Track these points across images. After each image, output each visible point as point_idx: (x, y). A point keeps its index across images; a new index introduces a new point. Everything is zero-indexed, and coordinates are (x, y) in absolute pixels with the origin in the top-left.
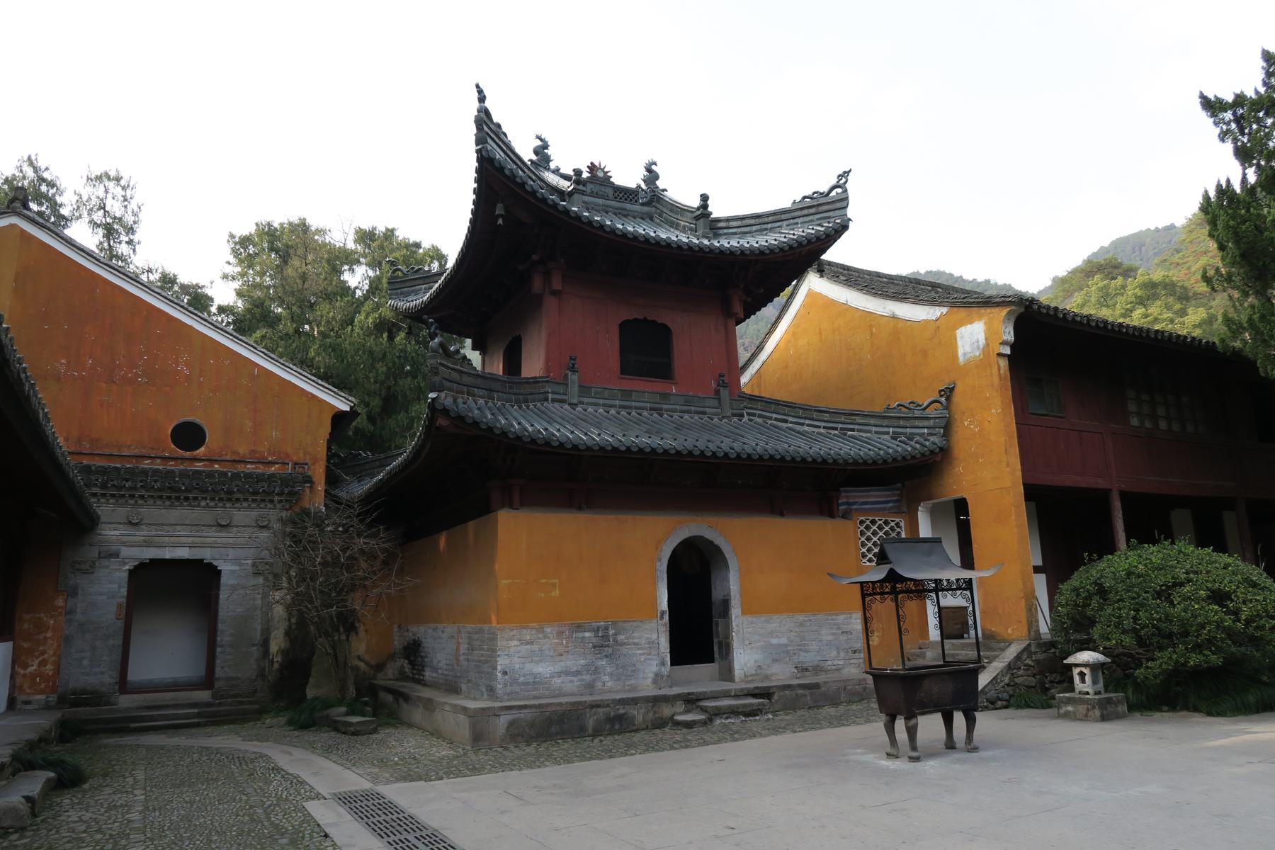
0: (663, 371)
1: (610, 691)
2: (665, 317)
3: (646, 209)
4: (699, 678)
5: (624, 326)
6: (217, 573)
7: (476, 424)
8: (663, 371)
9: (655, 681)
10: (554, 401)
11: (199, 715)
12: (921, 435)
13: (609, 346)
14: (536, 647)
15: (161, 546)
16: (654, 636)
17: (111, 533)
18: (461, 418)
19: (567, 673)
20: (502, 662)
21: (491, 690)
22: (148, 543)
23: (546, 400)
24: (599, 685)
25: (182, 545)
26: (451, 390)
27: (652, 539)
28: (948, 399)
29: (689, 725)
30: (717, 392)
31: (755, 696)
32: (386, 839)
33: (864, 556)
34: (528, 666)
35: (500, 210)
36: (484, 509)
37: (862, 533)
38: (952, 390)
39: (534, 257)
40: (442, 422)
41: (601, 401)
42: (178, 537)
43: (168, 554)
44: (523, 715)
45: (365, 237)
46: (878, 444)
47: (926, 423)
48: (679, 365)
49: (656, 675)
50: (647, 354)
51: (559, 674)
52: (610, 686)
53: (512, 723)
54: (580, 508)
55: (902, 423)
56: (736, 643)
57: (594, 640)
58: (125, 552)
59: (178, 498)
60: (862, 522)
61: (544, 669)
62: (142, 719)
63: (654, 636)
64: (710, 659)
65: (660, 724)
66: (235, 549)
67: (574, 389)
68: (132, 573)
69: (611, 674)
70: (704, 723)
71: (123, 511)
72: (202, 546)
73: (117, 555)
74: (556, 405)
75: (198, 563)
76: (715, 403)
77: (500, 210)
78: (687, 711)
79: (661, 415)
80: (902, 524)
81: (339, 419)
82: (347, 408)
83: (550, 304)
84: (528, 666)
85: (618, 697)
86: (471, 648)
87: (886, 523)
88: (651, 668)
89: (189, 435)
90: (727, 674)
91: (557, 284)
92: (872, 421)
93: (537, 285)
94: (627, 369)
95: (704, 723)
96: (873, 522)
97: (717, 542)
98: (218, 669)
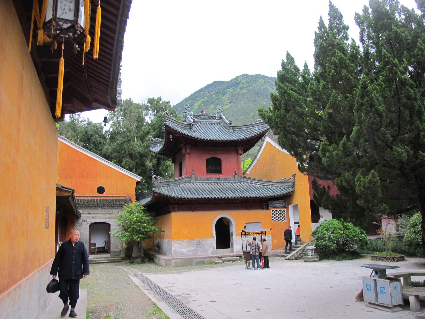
0: (219, 171)
1: (200, 255)
2: (219, 156)
3: (218, 121)
4: (224, 252)
5: (208, 160)
6: (109, 225)
7: (163, 195)
8: (219, 171)
9: (212, 253)
10: (188, 182)
11: (108, 260)
12: (287, 187)
13: (203, 166)
14: (181, 245)
15: (96, 219)
16: (212, 242)
17: (83, 216)
18: (160, 194)
19: (189, 251)
20: (173, 249)
21: (172, 255)
22: (93, 218)
23: (186, 182)
24: (197, 254)
25: (101, 218)
26: (158, 187)
27: (213, 217)
28: (294, 177)
29: (218, 263)
30: (234, 176)
31: (237, 256)
32: (196, 314)
33: (273, 220)
34: (180, 250)
35: (171, 137)
36: (170, 212)
37: (273, 214)
38: (295, 175)
39: (182, 145)
40: (156, 195)
41: (201, 181)
42: (100, 216)
43: (98, 221)
44: (179, 261)
45: (151, 101)
46: (277, 191)
47: (288, 184)
48: (223, 170)
49: (212, 251)
50: (214, 167)
51: (187, 251)
52: (200, 254)
53: (175, 263)
54: (193, 211)
55: (282, 184)
56: (234, 243)
57: (196, 243)
58: (88, 220)
59: (99, 207)
60: (273, 211)
61: (184, 250)
62: (93, 261)
63: (212, 242)
64: (229, 247)
65: (211, 263)
66: (114, 219)
67: (193, 179)
68: (90, 225)
69: (200, 251)
70: (221, 263)
71: (86, 211)
72: (106, 218)
73: (86, 221)
74: (188, 183)
75: (105, 223)
76: (234, 179)
77: (171, 137)
78: (218, 260)
79: (217, 184)
80: (285, 211)
81: (138, 183)
82: (140, 180)
83: (187, 157)
84: (180, 250)
85: (201, 256)
86: (168, 245)
87: (280, 210)
88: (211, 250)
89: (101, 190)
90: (232, 251)
91: (188, 151)
92: (275, 184)
93: (183, 151)
94: (209, 171)
95: (221, 263)
96: (276, 211)
97: (229, 218)
98: (111, 247)
